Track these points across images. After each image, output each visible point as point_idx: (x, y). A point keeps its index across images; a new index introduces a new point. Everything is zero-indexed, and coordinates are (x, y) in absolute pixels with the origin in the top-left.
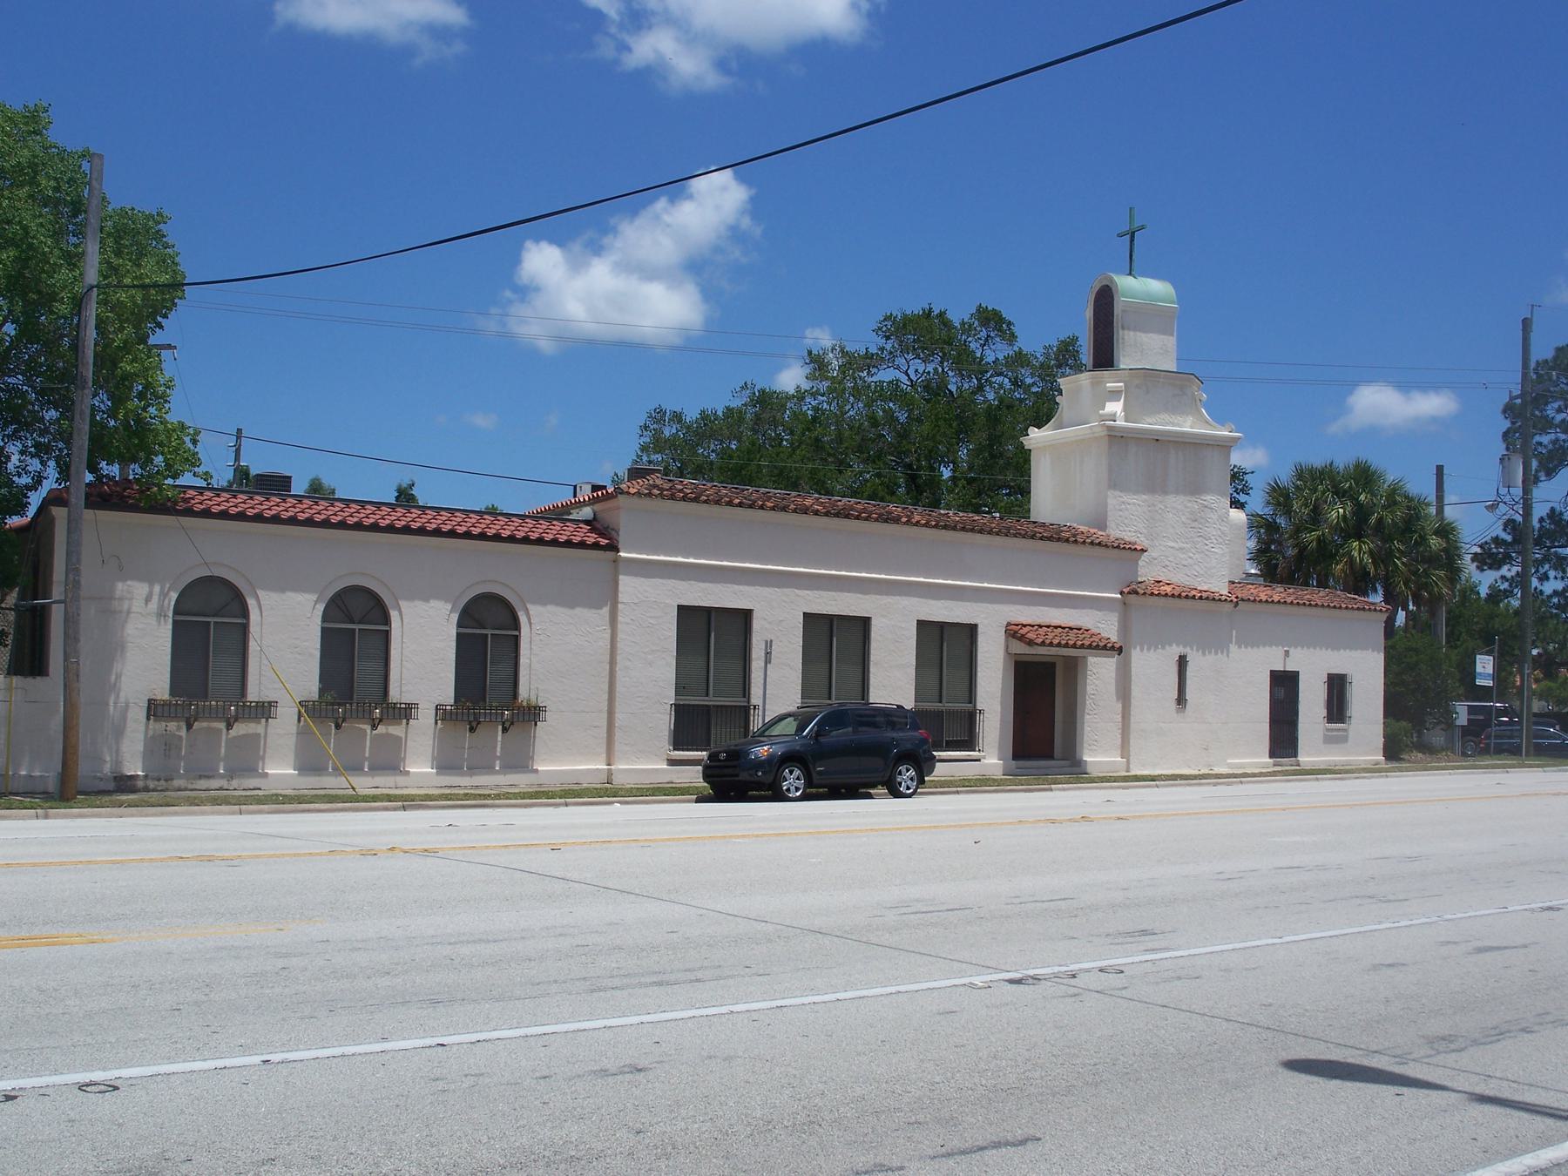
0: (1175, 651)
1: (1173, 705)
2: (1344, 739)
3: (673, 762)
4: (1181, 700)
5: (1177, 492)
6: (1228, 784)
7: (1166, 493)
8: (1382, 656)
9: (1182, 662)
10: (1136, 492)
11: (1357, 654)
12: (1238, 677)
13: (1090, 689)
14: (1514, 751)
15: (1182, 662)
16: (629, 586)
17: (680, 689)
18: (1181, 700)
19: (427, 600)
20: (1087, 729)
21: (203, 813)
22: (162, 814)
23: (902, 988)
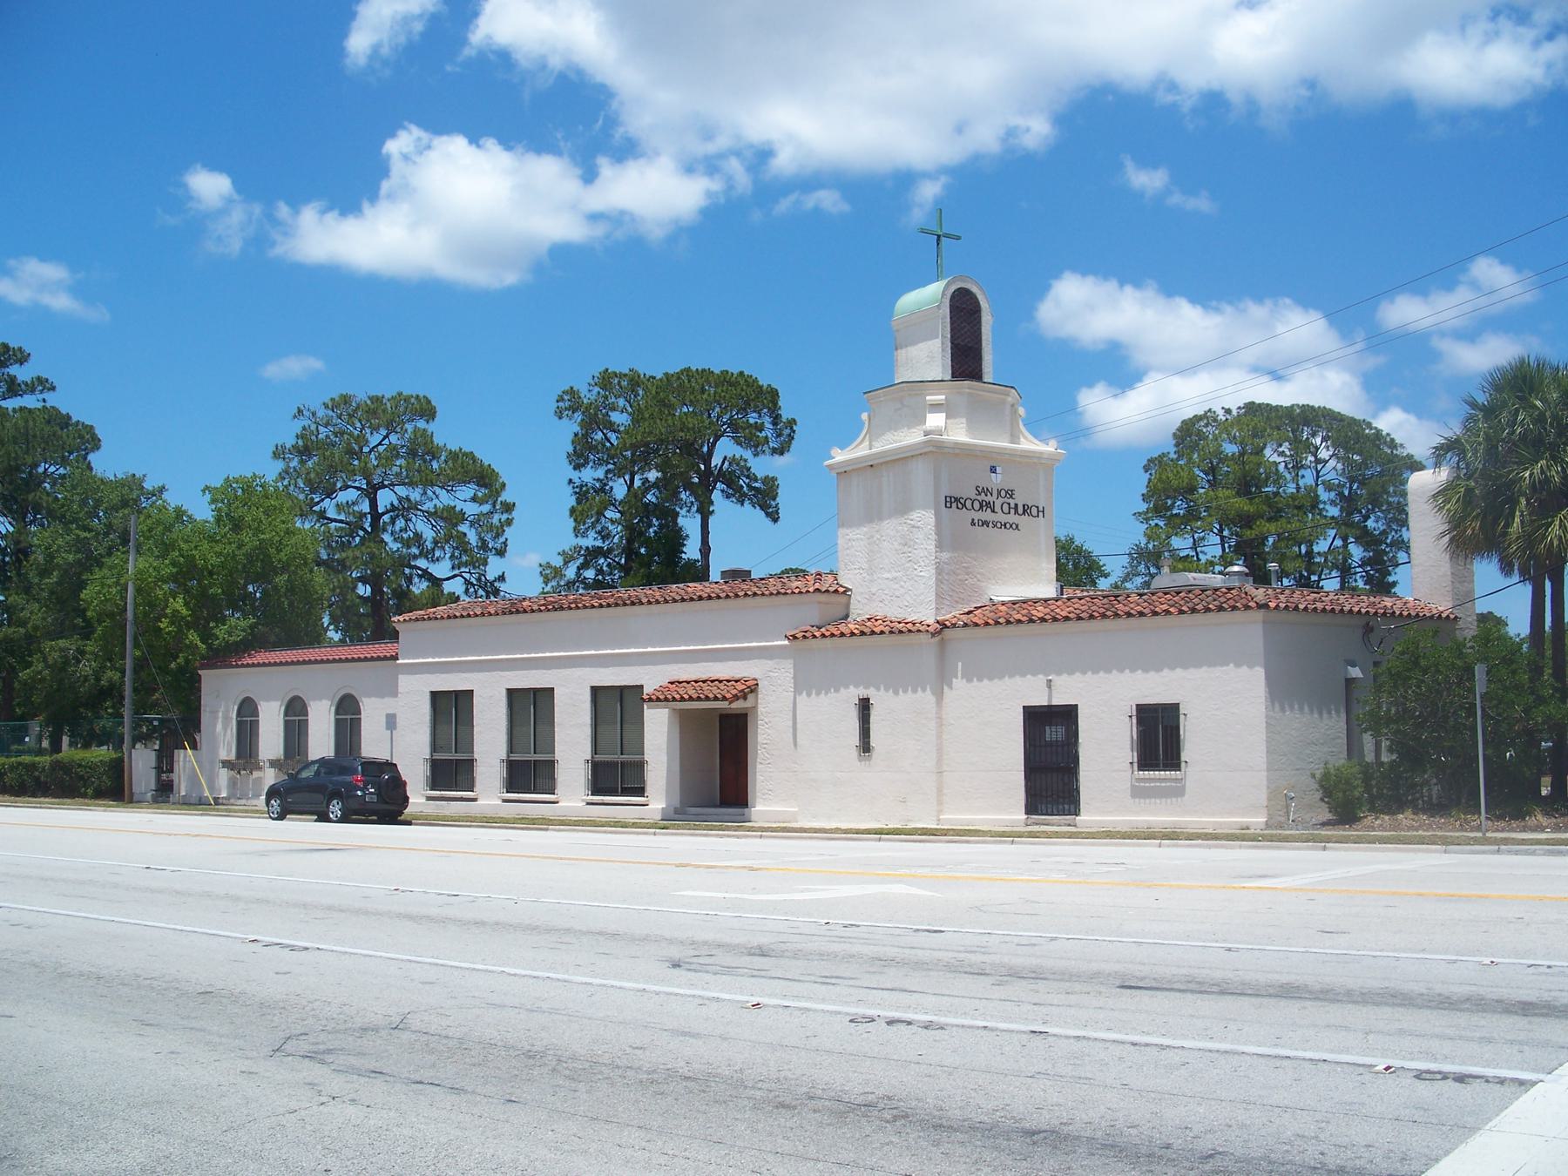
0: (853, 694)
1: (854, 753)
2: (1178, 791)
3: (429, 798)
4: (865, 746)
5: (890, 517)
6: (1533, 853)
7: (881, 519)
8: (1260, 672)
9: (865, 706)
10: (860, 525)
11: (1193, 673)
12: (984, 722)
13: (760, 739)
14: (84, 796)
15: (865, 706)
16: (405, 682)
17: (435, 747)
18: (865, 746)
19: (1023, 675)
20: (759, 778)
21: (1346, 850)
22: (1209, 847)
23: (1186, 1044)
